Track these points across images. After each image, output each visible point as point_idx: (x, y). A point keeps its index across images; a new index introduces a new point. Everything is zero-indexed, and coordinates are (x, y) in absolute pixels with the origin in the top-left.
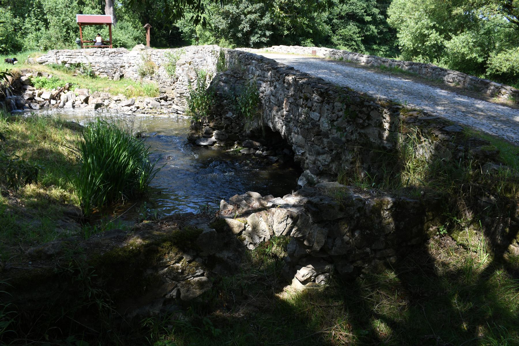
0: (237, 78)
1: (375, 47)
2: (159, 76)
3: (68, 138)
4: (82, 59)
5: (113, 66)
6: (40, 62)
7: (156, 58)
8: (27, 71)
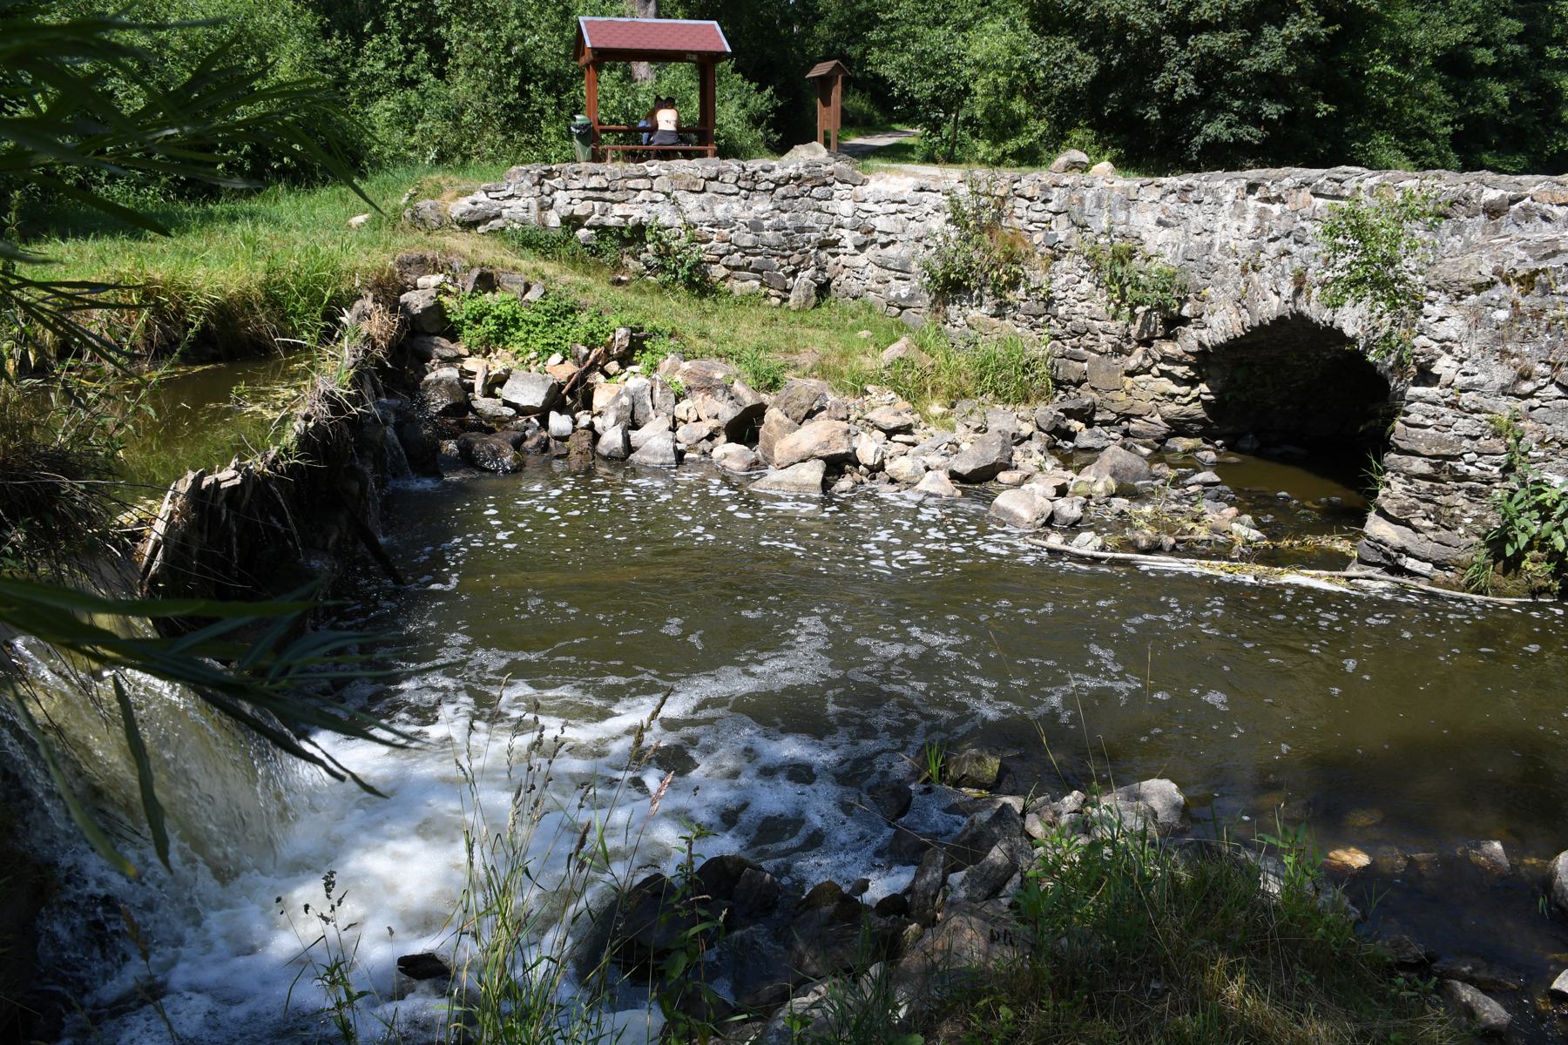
2: (1049, 302)
3: (200, 271)
4: (655, 207)
5: (791, 240)
6: (467, 218)
7: (1037, 216)
8: (424, 265)
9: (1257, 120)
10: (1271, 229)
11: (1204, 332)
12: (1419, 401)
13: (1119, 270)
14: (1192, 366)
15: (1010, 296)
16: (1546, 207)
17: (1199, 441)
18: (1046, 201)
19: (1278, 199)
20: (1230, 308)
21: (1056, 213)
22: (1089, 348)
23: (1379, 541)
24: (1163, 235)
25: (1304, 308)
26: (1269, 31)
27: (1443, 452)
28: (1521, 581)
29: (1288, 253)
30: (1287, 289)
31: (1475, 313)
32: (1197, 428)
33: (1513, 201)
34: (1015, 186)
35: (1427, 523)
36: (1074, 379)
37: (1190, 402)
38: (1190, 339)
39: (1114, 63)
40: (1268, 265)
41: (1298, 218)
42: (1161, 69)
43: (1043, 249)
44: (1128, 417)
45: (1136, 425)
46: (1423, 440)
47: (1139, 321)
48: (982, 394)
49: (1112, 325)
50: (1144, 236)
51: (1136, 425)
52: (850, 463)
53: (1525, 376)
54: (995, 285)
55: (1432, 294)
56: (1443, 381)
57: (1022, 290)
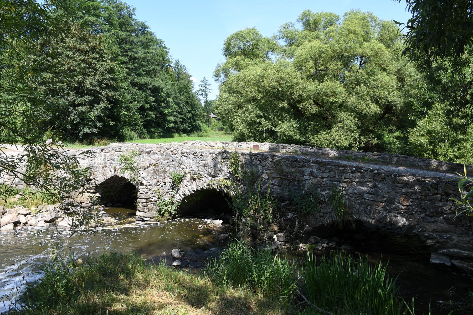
0: (289, 180)
1: (152, 130)
9: (96, 127)
14: (94, 189)
16: (156, 152)
19: (108, 152)
20: (101, 176)
26: (96, 105)
28: (165, 218)
30: (113, 171)
35: (147, 211)
44: (81, 203)
45: (83, 205)
46: (143, 196)
52: (19, 223)
53: (158, 182)
55: (140, 169)
56: (145, 184)
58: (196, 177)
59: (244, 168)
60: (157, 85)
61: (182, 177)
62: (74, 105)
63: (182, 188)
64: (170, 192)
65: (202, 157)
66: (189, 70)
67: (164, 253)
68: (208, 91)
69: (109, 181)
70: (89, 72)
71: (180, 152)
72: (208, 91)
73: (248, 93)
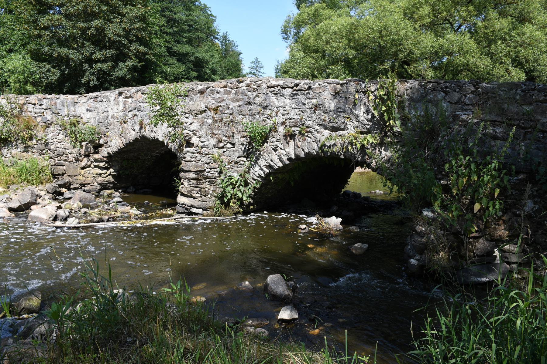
2: (47, 144)
7: (38, 111)
10: (129, 108)
11: (109, 149)
12: (188, 153)
13: (73, 129)
14: (106, 162)
15: (30, 143)
16: (217, 89)
17: (113, 190)
18: (41, 105)
19: (130, 97)
20: (118, 138)
21: (46, 109)
22: (65, 160)
23: (183, 204)
24: (89, 114)
25: (144, 134)
27: (199, 169)
29: (136, 115)
30: (137, 128)
31: (202, 121)
32: (111, 186)
33: (207, 88)
34: (27, 99)
35: (198, 195)
36: (60, 173)
37: (107, 176)
38: (104, 152)
39: (66, 72)
40: (129, 120)
41: (138, 102)
42: (84, 75)
43: (42, 124)
44: (84, 185)
45: (88, 188)
46: (191, 166)
47: (84, 148)
48: (21, 183)
49: (73, 151)
50: (82, 116)
51: (88, 188)
53: (220, 141)
54: (23, 139)
56: (195, 145)
57: (34, 140)
58: (297, 132)
59: (407, 109)
60: (201, 57)
61: (267, 131)
62: (90, 61)
63: (265, 154)
64: (241, 162)
65: (310, 91)
66: (239, 47)
67: (247, 283)
68: (260, 74)
69: (131, 148)
70: (112, 17)
71: (265, 86)
72: (260, 74)
73: (334, 49)
